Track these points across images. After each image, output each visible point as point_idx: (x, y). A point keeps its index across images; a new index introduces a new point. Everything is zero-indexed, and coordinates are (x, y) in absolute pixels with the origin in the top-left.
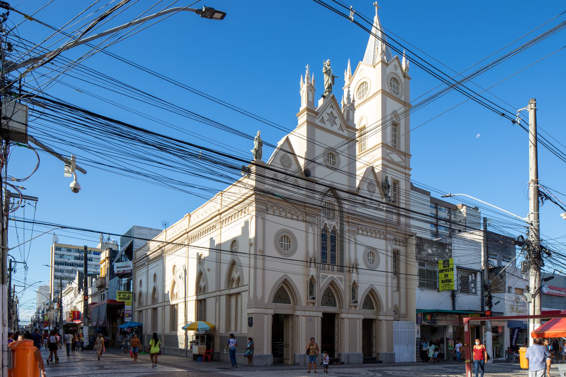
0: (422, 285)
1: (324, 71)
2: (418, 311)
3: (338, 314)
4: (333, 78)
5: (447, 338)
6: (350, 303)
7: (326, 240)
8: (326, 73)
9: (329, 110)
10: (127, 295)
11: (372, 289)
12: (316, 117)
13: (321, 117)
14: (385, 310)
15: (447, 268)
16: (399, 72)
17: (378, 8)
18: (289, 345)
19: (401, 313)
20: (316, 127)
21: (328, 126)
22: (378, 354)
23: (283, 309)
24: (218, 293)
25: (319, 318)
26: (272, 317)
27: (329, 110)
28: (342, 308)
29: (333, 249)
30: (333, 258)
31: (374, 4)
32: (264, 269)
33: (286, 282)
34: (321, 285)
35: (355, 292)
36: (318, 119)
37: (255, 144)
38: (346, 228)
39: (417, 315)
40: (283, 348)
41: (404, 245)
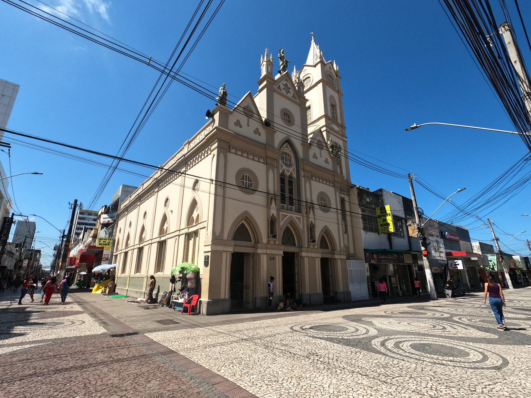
2: (365, 250)
3: (298, 253)
5: (389, 276)
6: (309, 242)
7: (284, 184)
10: (107, 241)
13: (278, 86)
14: (339, 249)
15: (384, 214)
17: (314, 37)
22: (336, 293)
23: (244, 248)
24: (177, 233)
25: (280, 256)
26: (231, 256)
28: (302, 247)
29: (291, 191)
30: (291, 199)
32: (168, 75)
34: (282, 223)
35: (312, 232)
38: (302, 173)
39: (365, 254)
40: (243, 289)
41: (348, 194)
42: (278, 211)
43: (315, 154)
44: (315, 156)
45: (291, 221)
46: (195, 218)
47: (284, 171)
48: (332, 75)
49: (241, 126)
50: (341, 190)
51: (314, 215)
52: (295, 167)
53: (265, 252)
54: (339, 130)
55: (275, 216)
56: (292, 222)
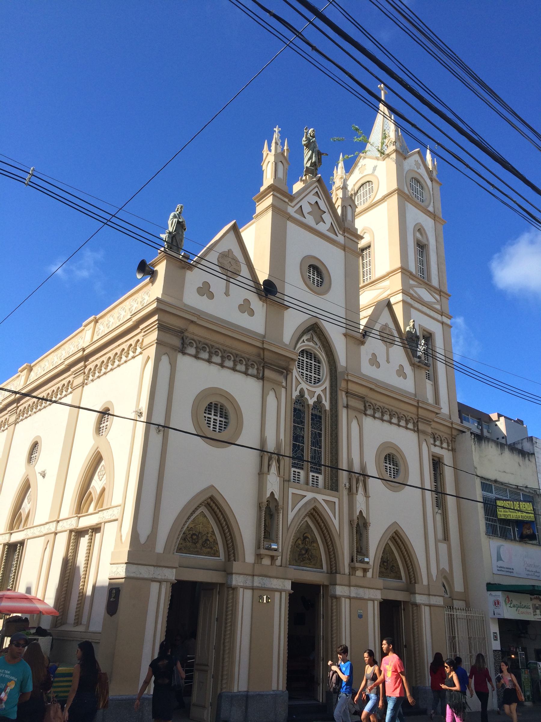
0: (487, 534)
1: (304, 143)
3: (326, 587)
4: (319, 154)
6: (352, 561)
7: (302, 423)
8: (307, 147)
9: (313, 199)
11: (396, 533)
12: (290, 203)
13: (298, 206)
14: (425, 582)
16: (422, 171)
18: (208, 666)
19: (456, 591)
20: (288, 219)
21: (310, 220)
25: (283, 594)
26: (169, 589)
27: (313, 199)
28: (336, 573)
29: (316, 441)
31: (379, 86)
33: (212, 503)
34: (291, 515)
36: (293, 207)
37: (170, 225)
38: (342, 398)
41: (450, 448)
42: (285, 482)
43: (374, 355)
44: (374, 361)
45: (314, 509)
46: (95, 496)
47: (302, 392)
48: (421, 180)
49: (211, 296)
50: (434, 438)
51: (367, 496)
52: (327, 384)
53: (249, 584)
54: (434, 300)
55: (277, 497)
56: (316, 512)
